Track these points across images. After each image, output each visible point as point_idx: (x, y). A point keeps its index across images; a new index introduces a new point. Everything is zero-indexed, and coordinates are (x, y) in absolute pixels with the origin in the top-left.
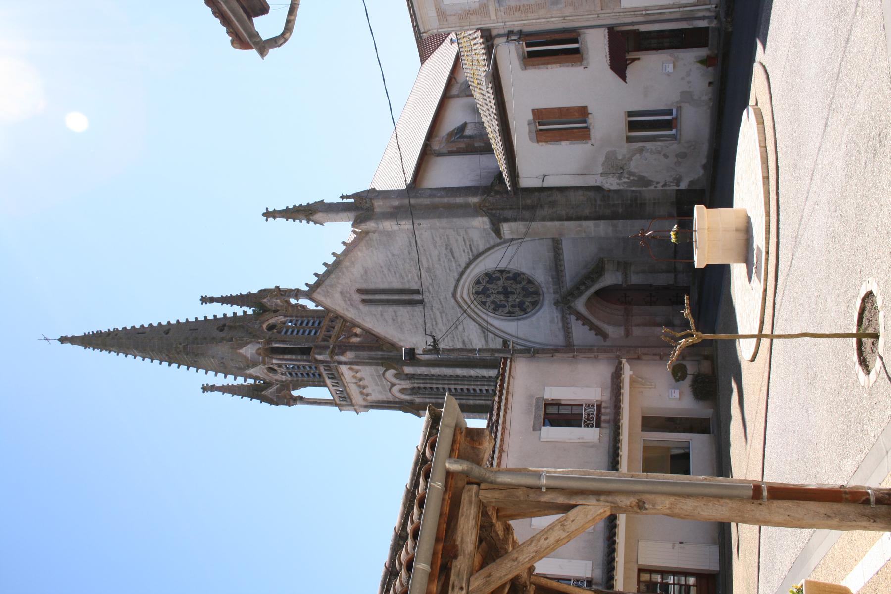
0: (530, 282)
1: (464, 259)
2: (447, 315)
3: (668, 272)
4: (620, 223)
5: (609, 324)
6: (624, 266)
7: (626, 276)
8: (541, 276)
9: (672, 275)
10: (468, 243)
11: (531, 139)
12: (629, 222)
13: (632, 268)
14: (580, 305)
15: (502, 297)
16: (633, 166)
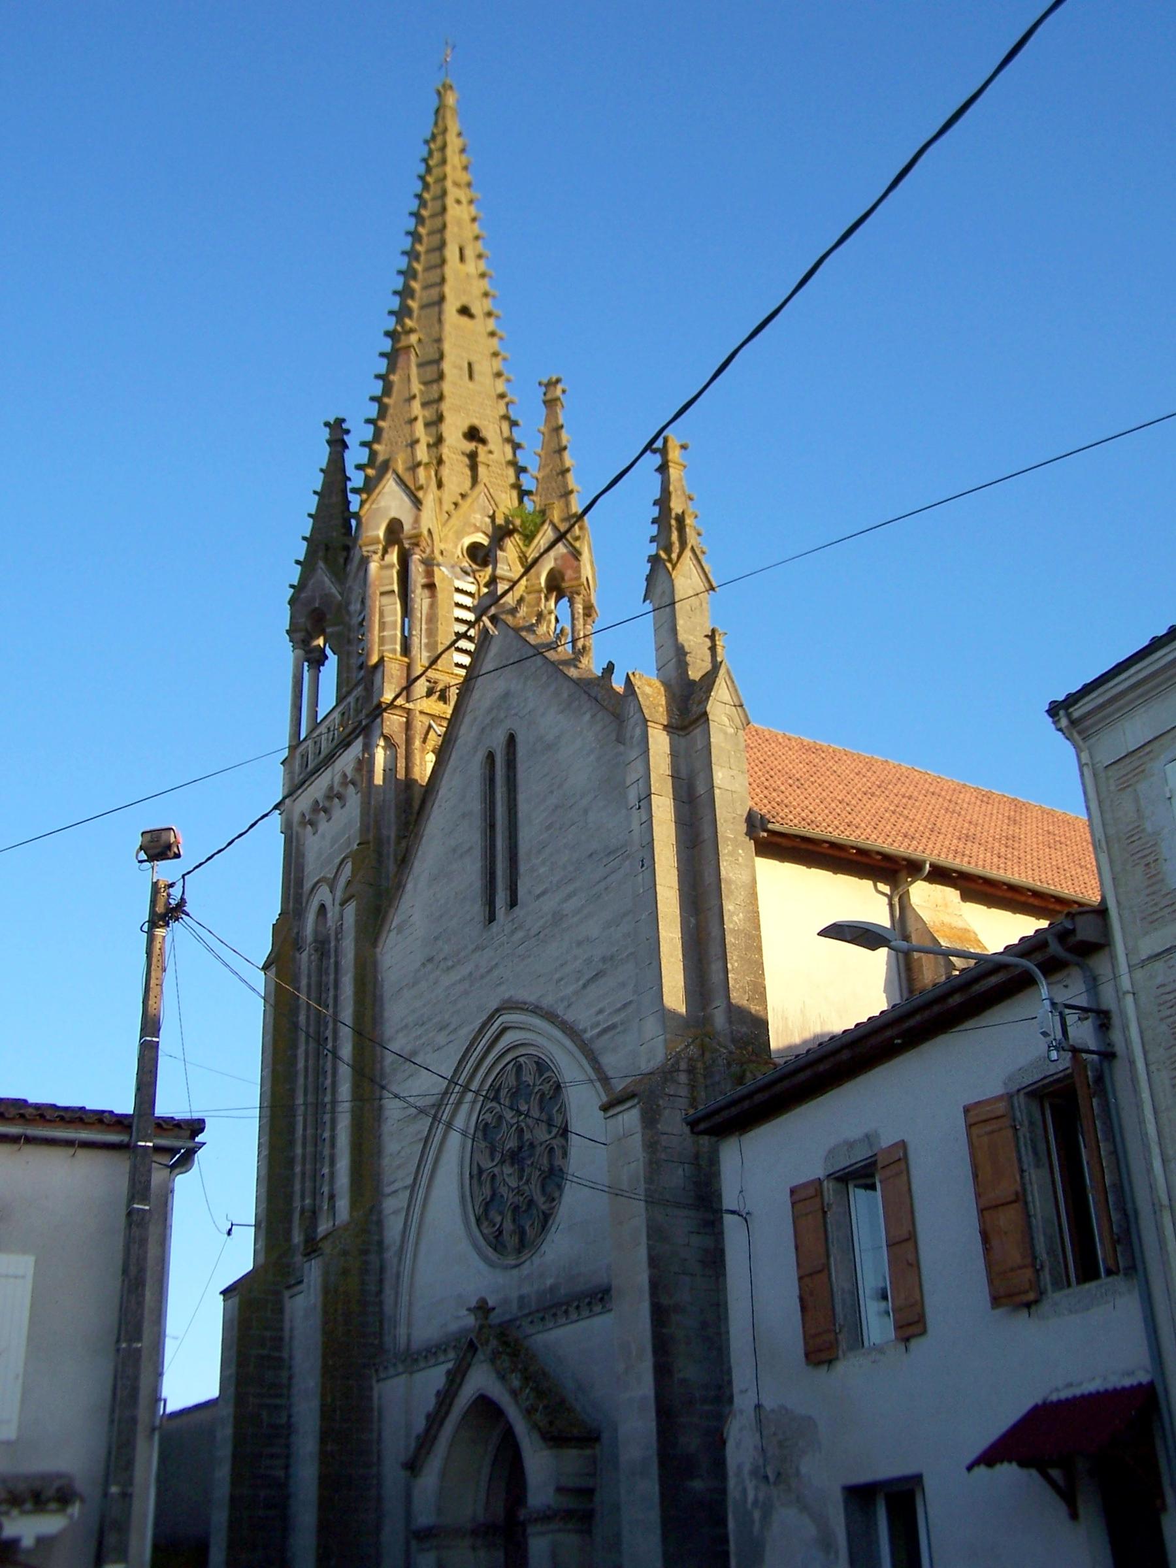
1: (582, 1016)
2: (466, 993)
4: (650, 1487)
5: (443, 1474)
7: (547, 1516)
11: (832, 1153)
14: (481, 1380)
15: (512, 1144)
16: (786, 1517)
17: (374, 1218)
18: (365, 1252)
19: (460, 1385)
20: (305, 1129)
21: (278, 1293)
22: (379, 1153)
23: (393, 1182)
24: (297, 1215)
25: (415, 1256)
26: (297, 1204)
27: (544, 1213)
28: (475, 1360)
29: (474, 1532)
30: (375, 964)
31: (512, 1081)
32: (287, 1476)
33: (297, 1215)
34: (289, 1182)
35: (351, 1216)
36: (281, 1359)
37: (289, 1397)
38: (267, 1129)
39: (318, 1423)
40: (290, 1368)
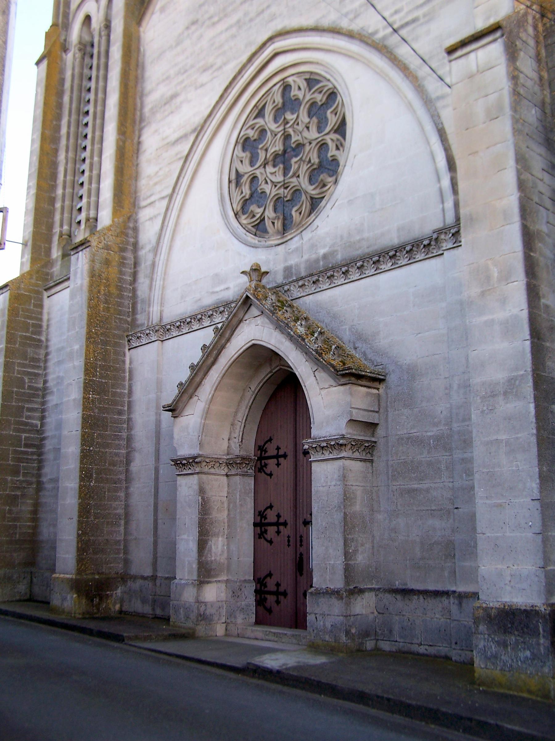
0: (315, 204)
2: (234, 37)
3: (348, 570)
5: (207, 413)
6: (364, 440)
7: (335, 445)
8: (335, 225)
9: (338, 583)
10: (419, 13)
12: (528, 434)
13: (357, 466)
15: (278, 147)
17: (131, 225)
18: (123, 250)
19: (228, 340)
20: (65, 176)
21: (39, 293)
22: (136, 177)
23: (151, 195)
24: (56, 238)
25: (170, 248)
26: (57, 229)
27: (312, 198)
28: (246, 317)
29: (229, 464)
30: (139, 39)
31: (279, 99)
32: (42, 425)
33: (56, 238)
34: (51, 214)
35: (113, 221)
36: (40, 341)
37: (45, 368)
38: (36, 175)
39: (82, 376)
40: (47, 347)
